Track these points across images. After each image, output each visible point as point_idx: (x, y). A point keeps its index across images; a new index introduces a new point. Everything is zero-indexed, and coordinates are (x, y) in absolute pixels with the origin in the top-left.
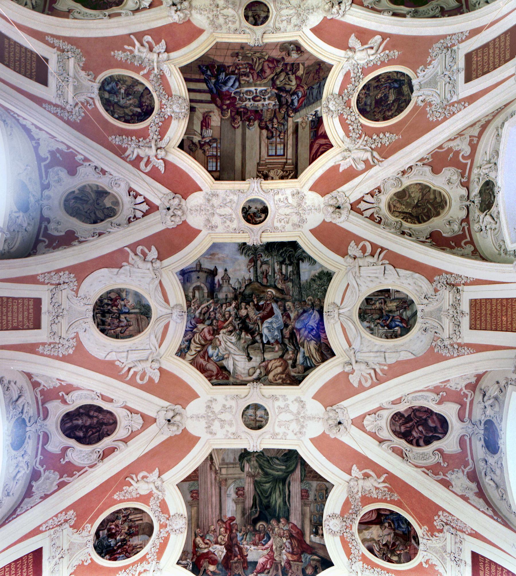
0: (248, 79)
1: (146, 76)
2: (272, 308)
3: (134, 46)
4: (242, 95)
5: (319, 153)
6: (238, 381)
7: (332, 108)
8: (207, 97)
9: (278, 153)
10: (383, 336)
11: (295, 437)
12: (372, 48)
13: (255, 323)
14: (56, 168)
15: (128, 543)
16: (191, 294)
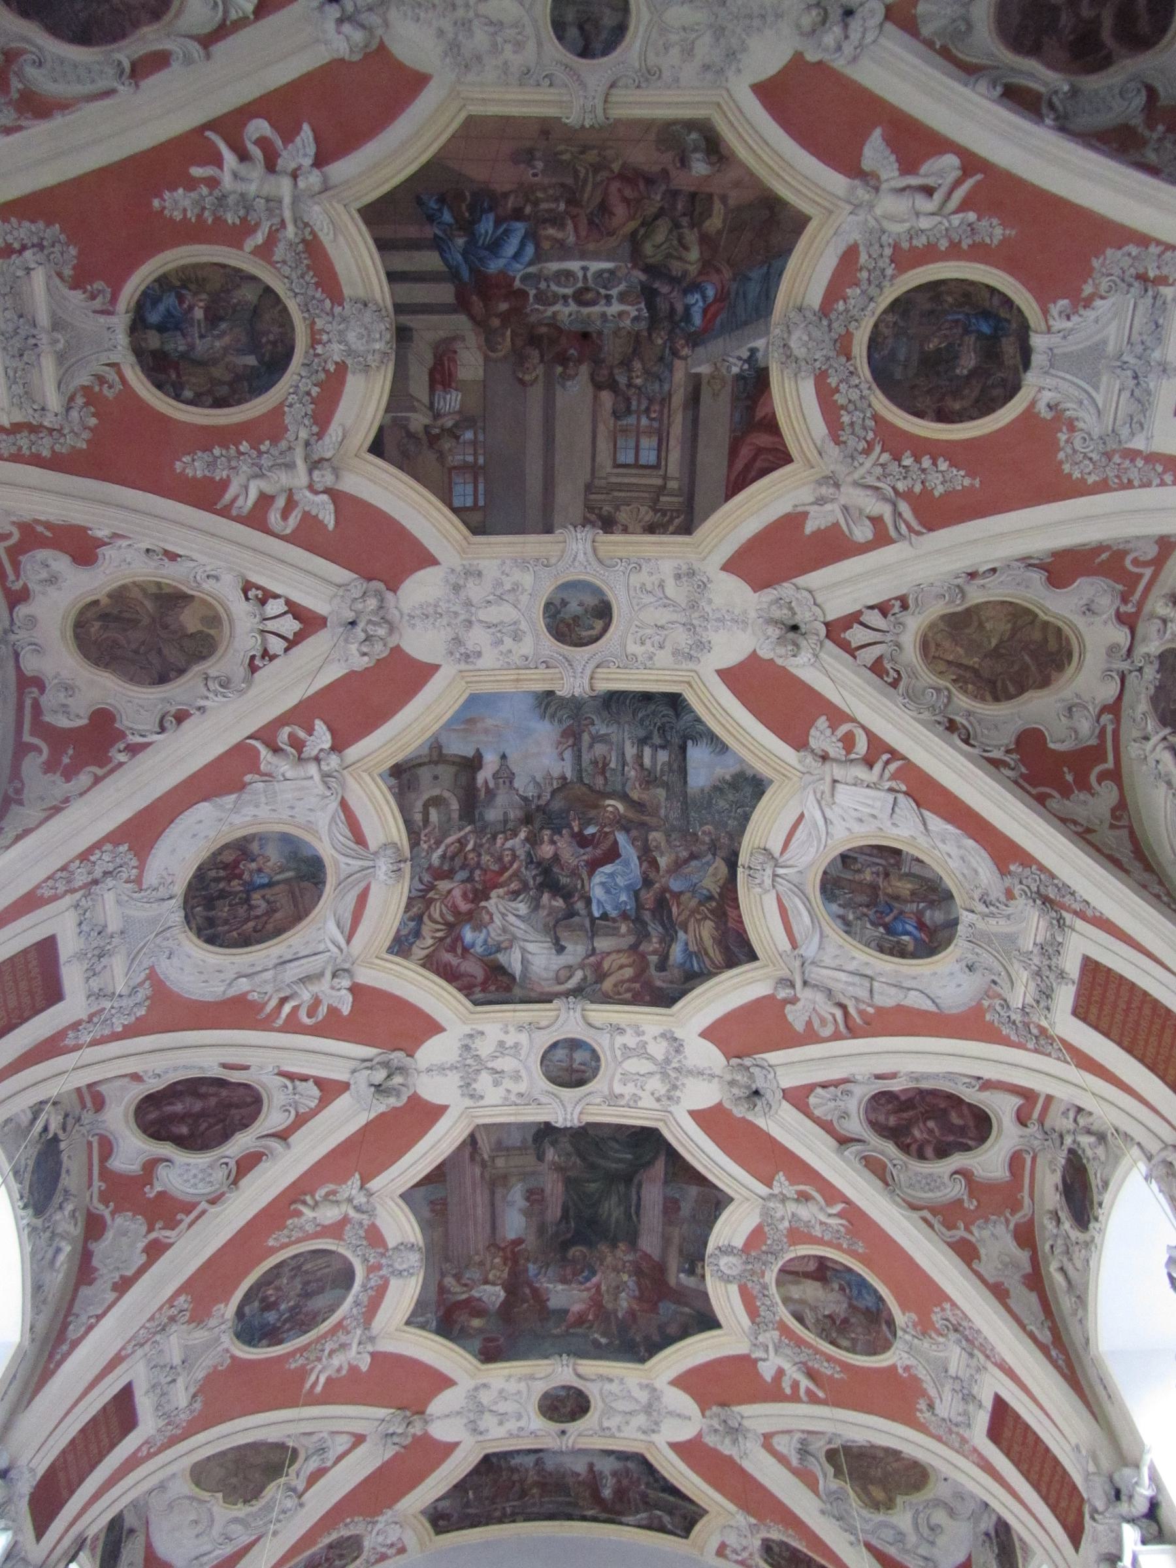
0: (560, 235)
1: (264, 252)
2: (616, 843)
3: (218, 161)
4: (543, 285)
5: (753, 473)
6: (533, 995)
7: (799, 351)
8: (445, 293)
9: (642, 462)
10: (873, 944)
11: (657, 1106)
12: (929, 191)
13: (574, 873)
14: (42, 554)
15: (304, 1310)
16: (418, 817)
